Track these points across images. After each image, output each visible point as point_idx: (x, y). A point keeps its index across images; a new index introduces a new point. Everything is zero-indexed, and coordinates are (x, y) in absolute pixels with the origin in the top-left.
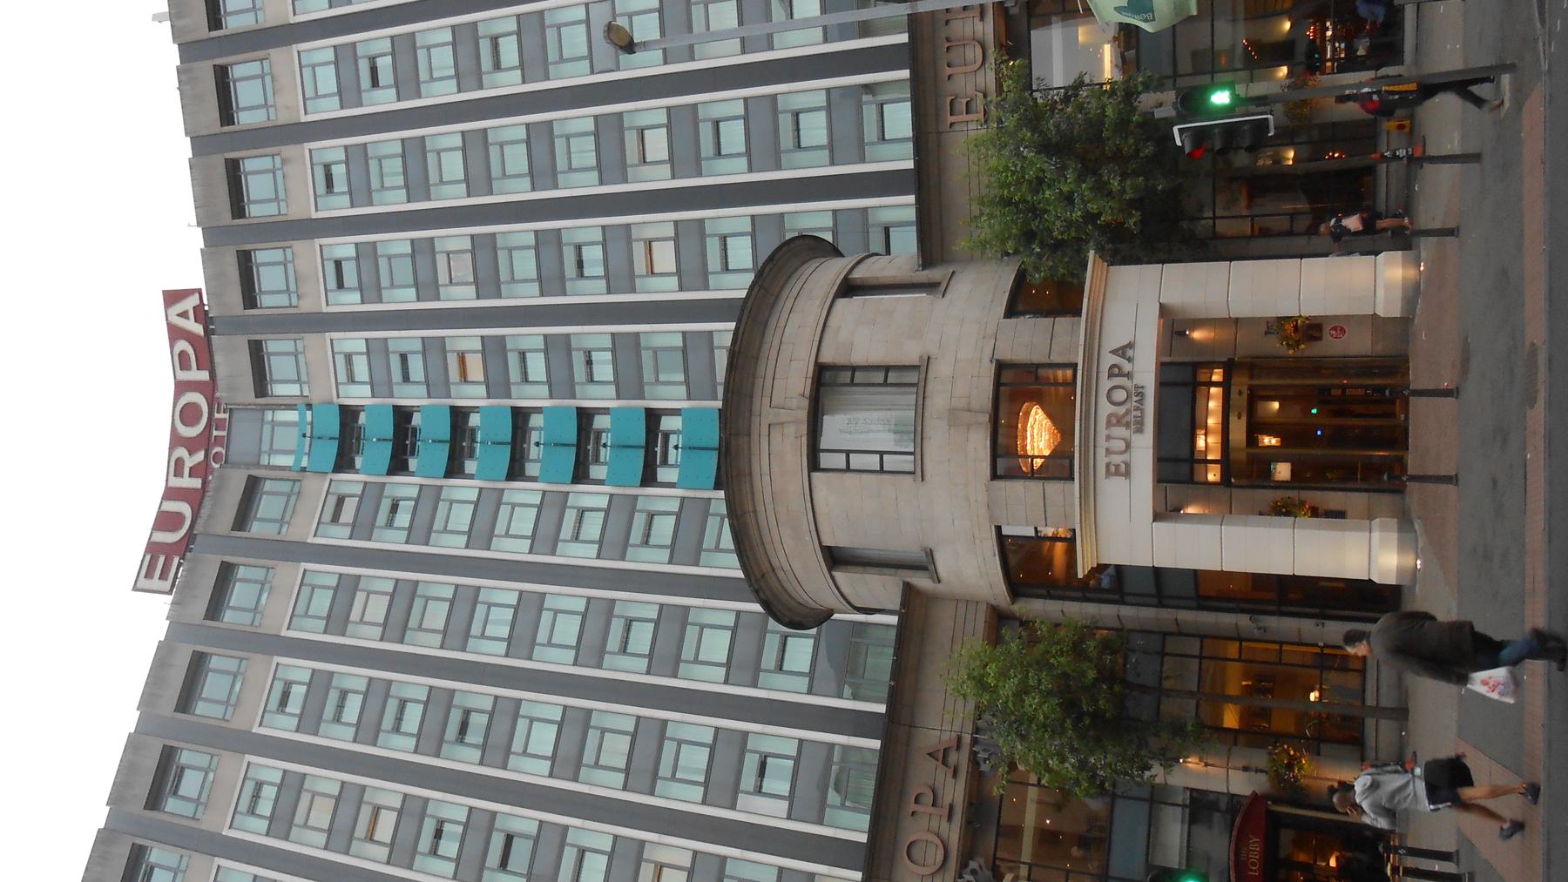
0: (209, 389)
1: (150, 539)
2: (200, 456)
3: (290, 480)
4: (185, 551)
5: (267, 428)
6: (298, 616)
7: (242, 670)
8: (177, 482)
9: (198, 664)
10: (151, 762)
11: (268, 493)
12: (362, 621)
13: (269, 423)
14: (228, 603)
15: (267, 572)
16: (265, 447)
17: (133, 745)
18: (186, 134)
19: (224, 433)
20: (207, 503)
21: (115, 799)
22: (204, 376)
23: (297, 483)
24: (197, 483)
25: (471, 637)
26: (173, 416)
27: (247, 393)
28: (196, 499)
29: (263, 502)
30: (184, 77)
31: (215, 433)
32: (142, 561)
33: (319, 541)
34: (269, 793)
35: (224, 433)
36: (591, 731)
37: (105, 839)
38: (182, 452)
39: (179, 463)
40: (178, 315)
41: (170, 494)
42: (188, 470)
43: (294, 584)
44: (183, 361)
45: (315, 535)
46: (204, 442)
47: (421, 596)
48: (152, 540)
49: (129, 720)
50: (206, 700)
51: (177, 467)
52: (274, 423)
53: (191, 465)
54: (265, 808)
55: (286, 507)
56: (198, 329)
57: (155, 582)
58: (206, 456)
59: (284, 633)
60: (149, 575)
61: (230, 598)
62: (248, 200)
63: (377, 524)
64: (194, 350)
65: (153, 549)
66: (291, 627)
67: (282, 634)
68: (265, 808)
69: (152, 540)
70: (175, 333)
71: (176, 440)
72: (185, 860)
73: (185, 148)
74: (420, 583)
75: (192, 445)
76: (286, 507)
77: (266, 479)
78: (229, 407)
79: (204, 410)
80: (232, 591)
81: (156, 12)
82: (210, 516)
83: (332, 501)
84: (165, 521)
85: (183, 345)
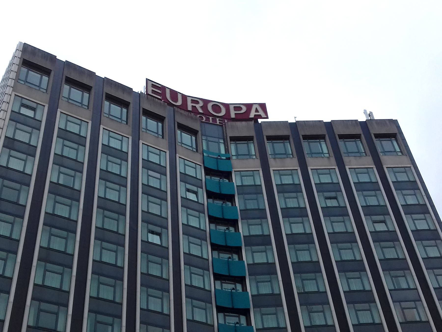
0: (227, 116)
1: (167, 87)
2: (201, 111)
3: (88, 104)
4: (167, 103)
5: (216, 140)
6: (22, 100)
7: (84, 106)
8: (189, 100)
9: (46, 72)
10: (85, 81)
11: (41, 78)
12: (149, 175)
13: (219, 141)
14: (31, 71)
15: (45, 90)
16: (210, 139)
17: (91, 74)
18: (331, 120)
19: (211, 122)
20: (183, 112)
21: (68, 64)
22: (233, 116)
23: (86, 107)
24: (190, 108)
25: (103, 211)
26: (216, 102)
27: (230, 133)
28: (184, 106)
29: (155, 122)
30: (354, 122)
31: (211, 118)
32: (158, 84)
33: (58, 113)
34: (30, 113)
35: (211, 122)
36: (114, 281)
37: (52, 58)
38: (201, 104)
39: (197, 102)
40: (256, 108)
41: (185, 97)
42: (195, 105)
43: (159, 147)
44: (237, 107)
45: (104, 128)
46: (207, 113)
47: (27, 158)
48: (166, 88)
49: (101, 73)
50: (28, 72)
51: (195, 101)
52: (219, 143)
53: (197, 107)
54: (24, 111)
55: (116, 117)
56: (252, 115)
57: (150, 89)
58: (201, 113)
59: (59, 110)
60: (153, 86)
61: (185, 133)
62: (310, 142)
63: (109, 156)
64: (242, 113)
65: (163, 88)
66: (17, 97)
67: (58, 109)
68: (24, 111)
69: (166, 88)
70: (249, 106)
71: (206, 102)
72: (105, 115)
73: (327, 119)
74: (33, 158)
75: (204, 107)
76: (116, 117)
77: (89, 94)
78: (224, 125)
79: (219, 114)
80: (153, 120)
81: (398, 120)
82: (181, 114)
83: (34, 105)
84: (174, 94)
85: (244, 109)
